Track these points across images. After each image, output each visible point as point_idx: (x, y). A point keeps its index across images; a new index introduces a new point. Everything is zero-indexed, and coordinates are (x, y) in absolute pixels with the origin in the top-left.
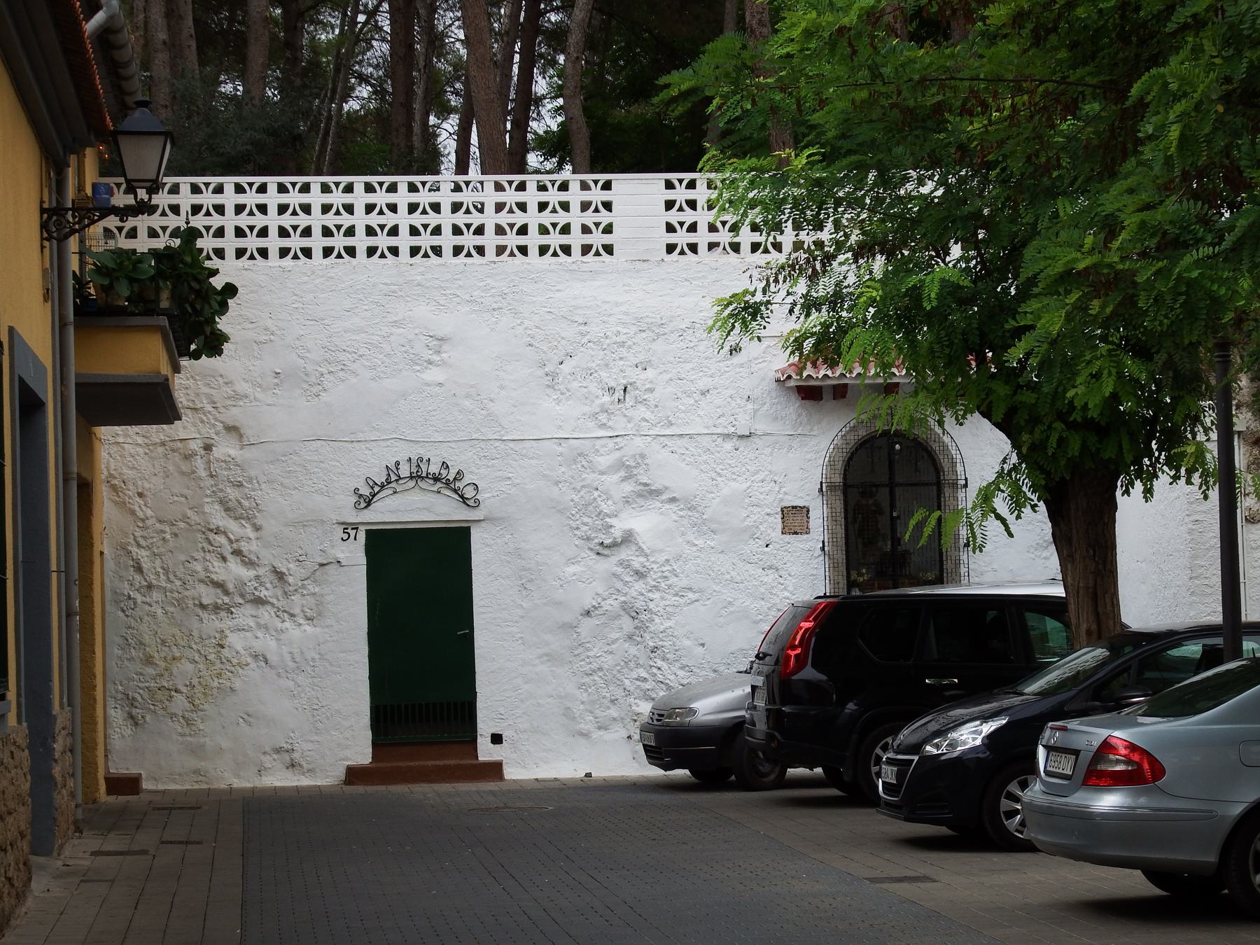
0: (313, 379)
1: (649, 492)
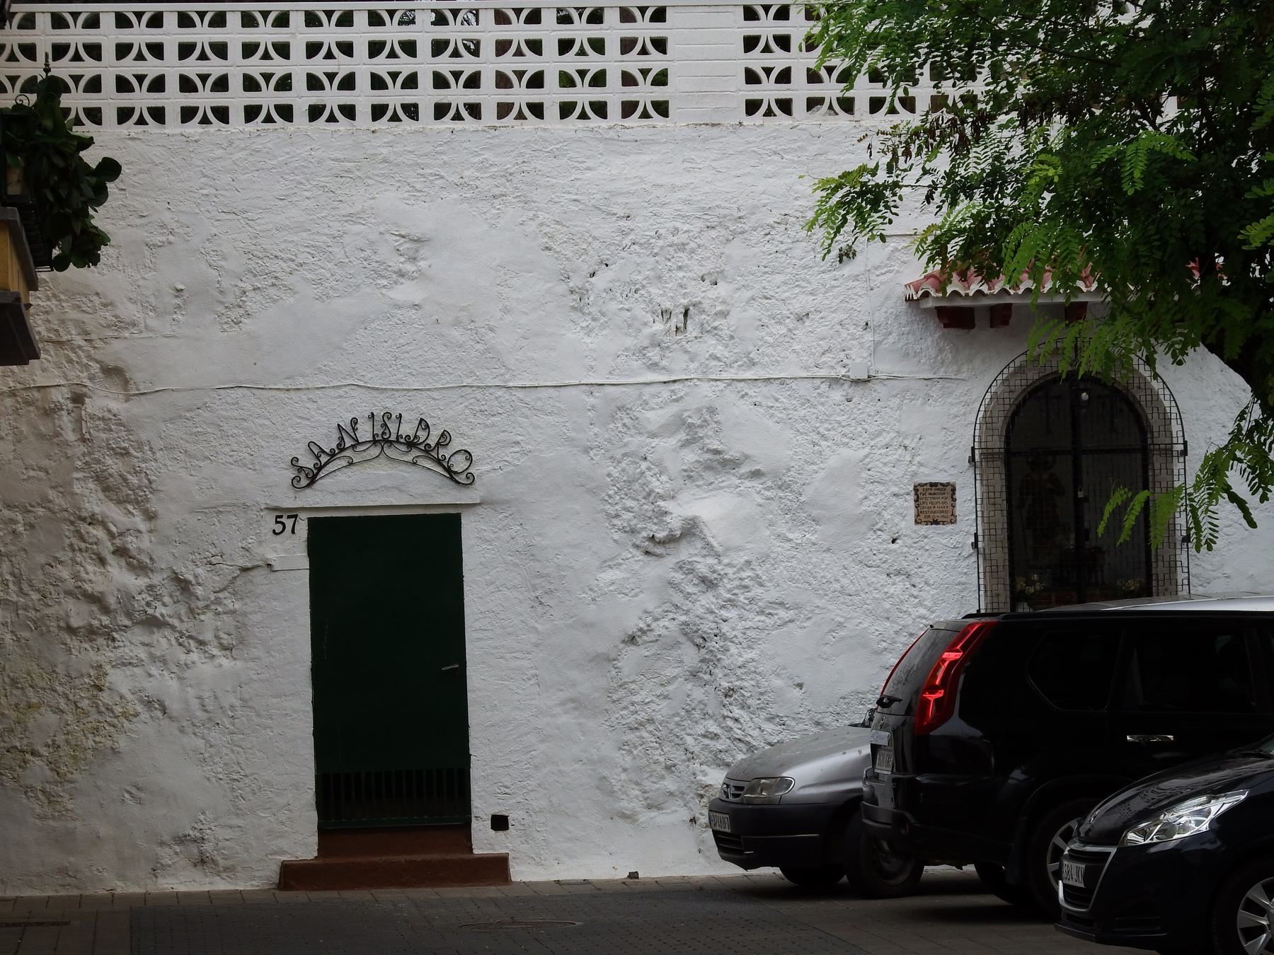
0: (230, 299)
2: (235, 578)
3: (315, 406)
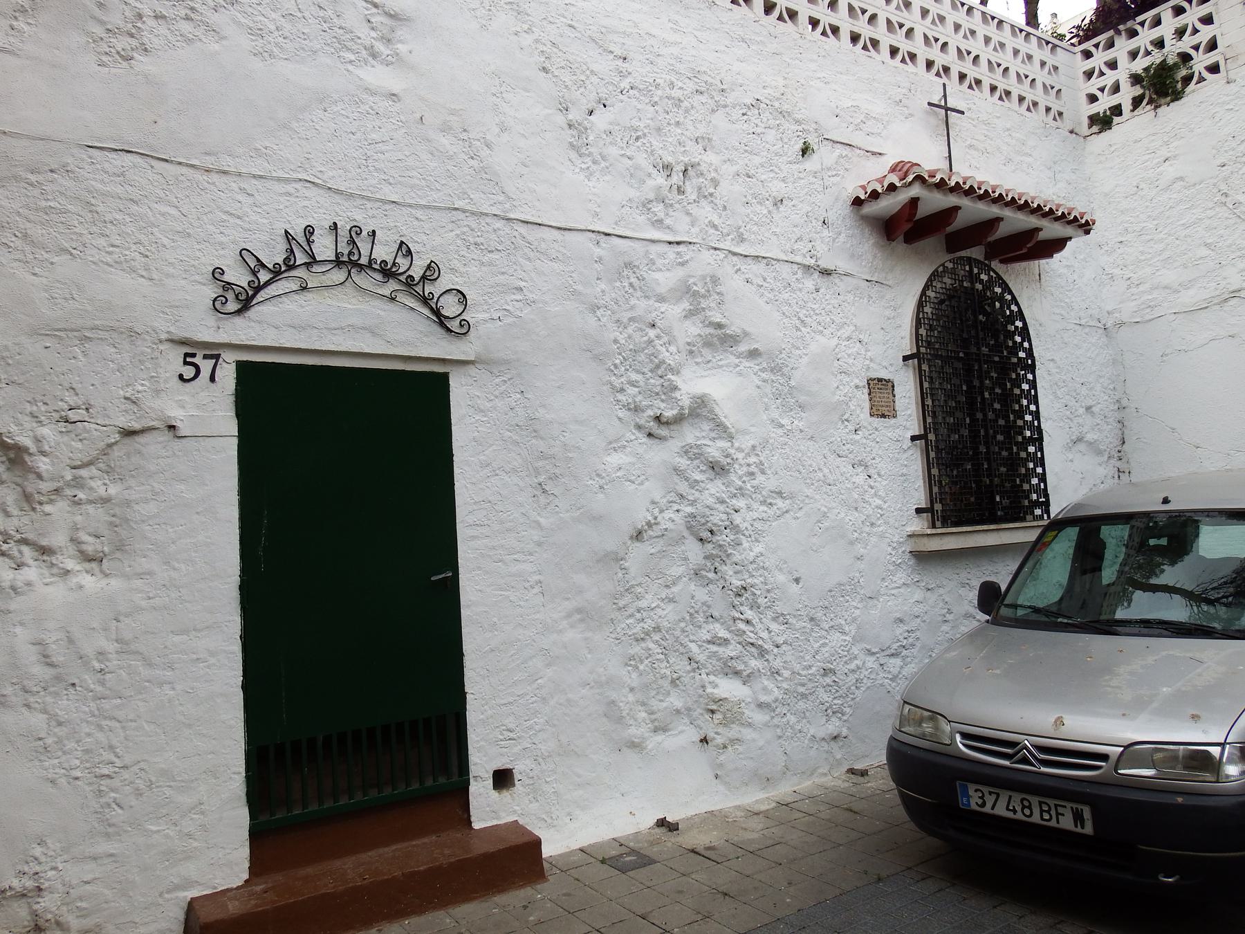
0: (115, 20)
1: (721, 339)
2: (110, 446)
3: (250, 200)
